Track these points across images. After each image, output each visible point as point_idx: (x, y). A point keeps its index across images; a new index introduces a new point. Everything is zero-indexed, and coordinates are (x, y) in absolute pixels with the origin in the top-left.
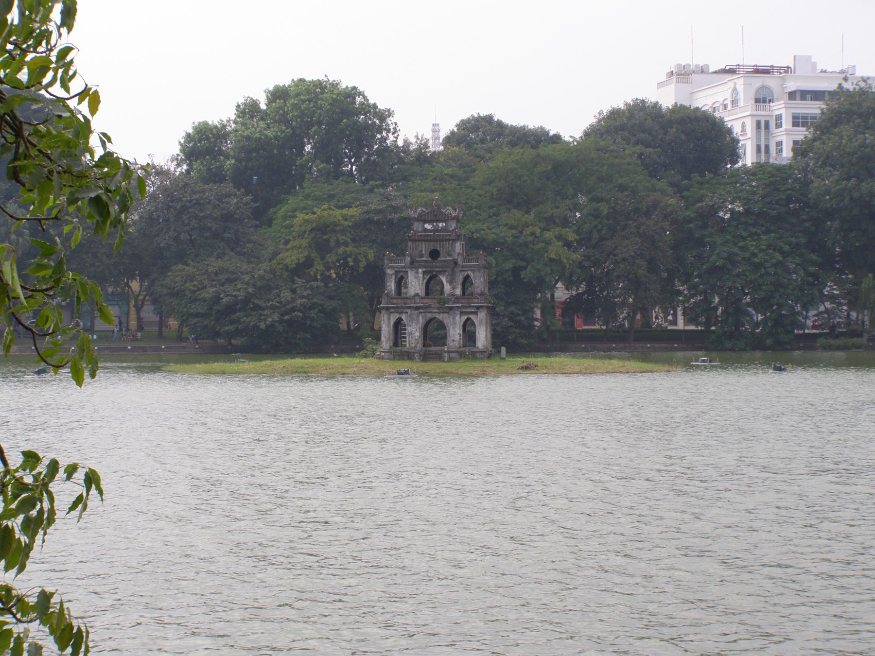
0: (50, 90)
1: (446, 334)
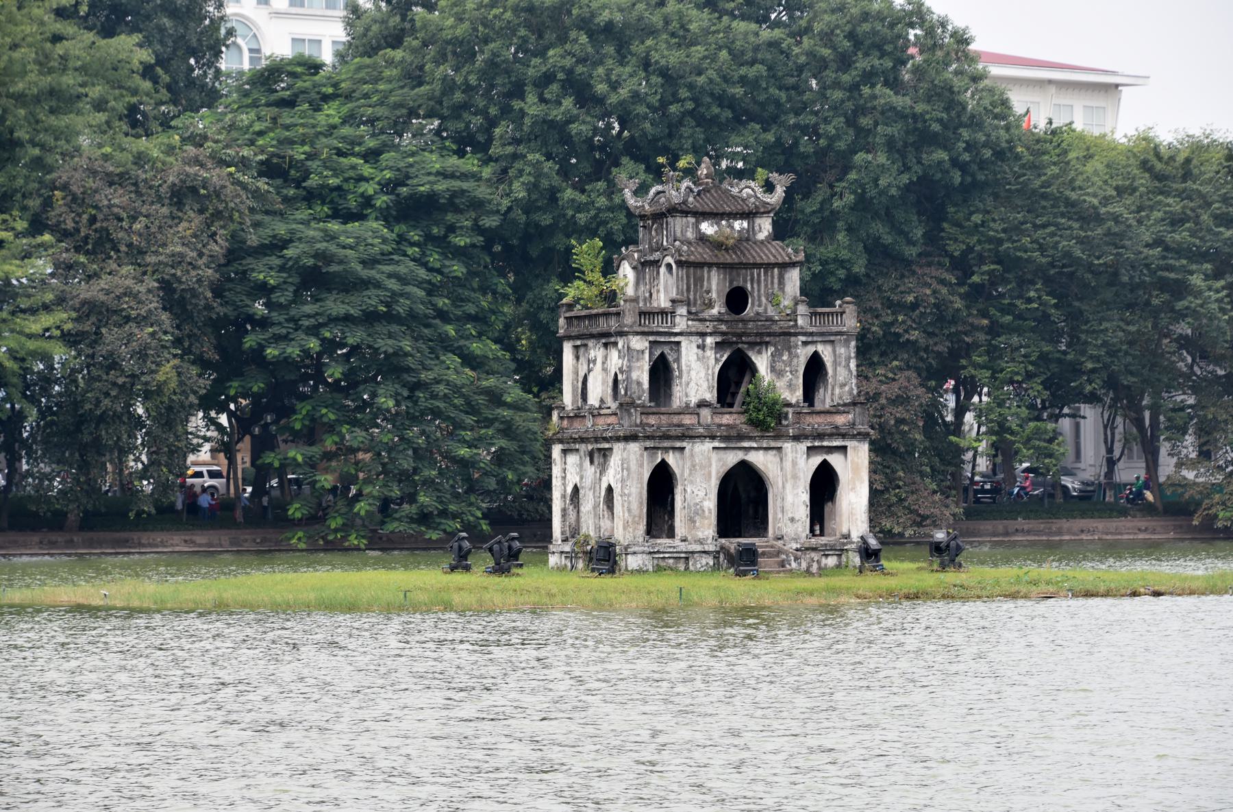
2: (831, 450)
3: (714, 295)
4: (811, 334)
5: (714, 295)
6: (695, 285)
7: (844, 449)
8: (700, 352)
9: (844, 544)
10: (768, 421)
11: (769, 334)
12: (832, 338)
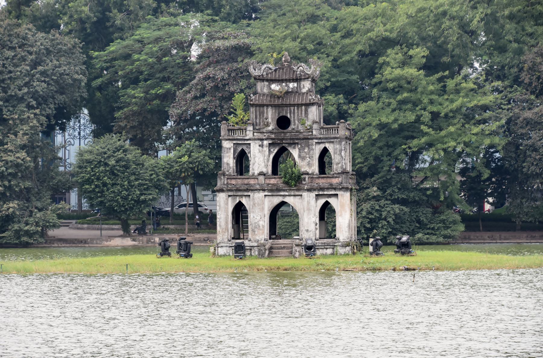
0: (318, 120)
1: (298, 223)
2: (330, 196)
3: (270, 120)
4: (320, 138)
5: (270, 120)
6: (260, 115)
8: (261, 148)
9: (335, 243)
10: (295, 182)
11: (297, 139)
12: (332, 140)
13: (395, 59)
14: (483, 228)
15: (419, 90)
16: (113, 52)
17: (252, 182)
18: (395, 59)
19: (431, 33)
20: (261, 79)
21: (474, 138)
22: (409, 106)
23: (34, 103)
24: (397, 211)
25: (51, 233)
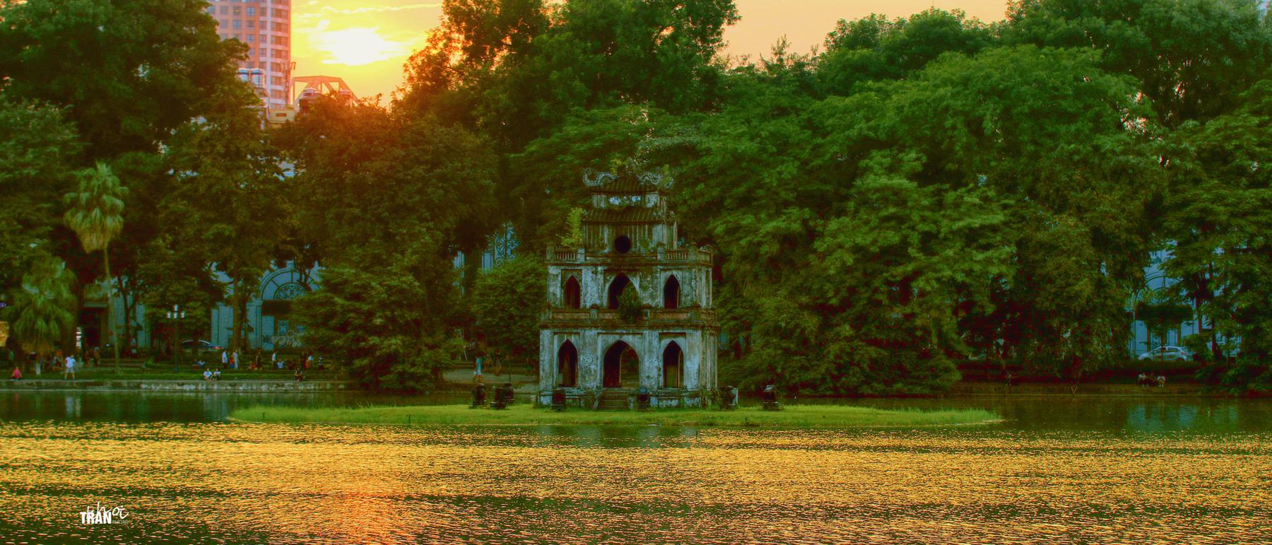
7: (683, 334)
10: (634, 316)
13: (881, 164)
14: (978, 380)
15: (910, 204)
16: (533, 152)
17: (583, 316)
18: (881, 164)
19: (928, 133)
20: (597, 190)
21: (977, 268)
22: (893, 223)
23: (427, 214)
24: (874, 355)
25: (449, 376)
